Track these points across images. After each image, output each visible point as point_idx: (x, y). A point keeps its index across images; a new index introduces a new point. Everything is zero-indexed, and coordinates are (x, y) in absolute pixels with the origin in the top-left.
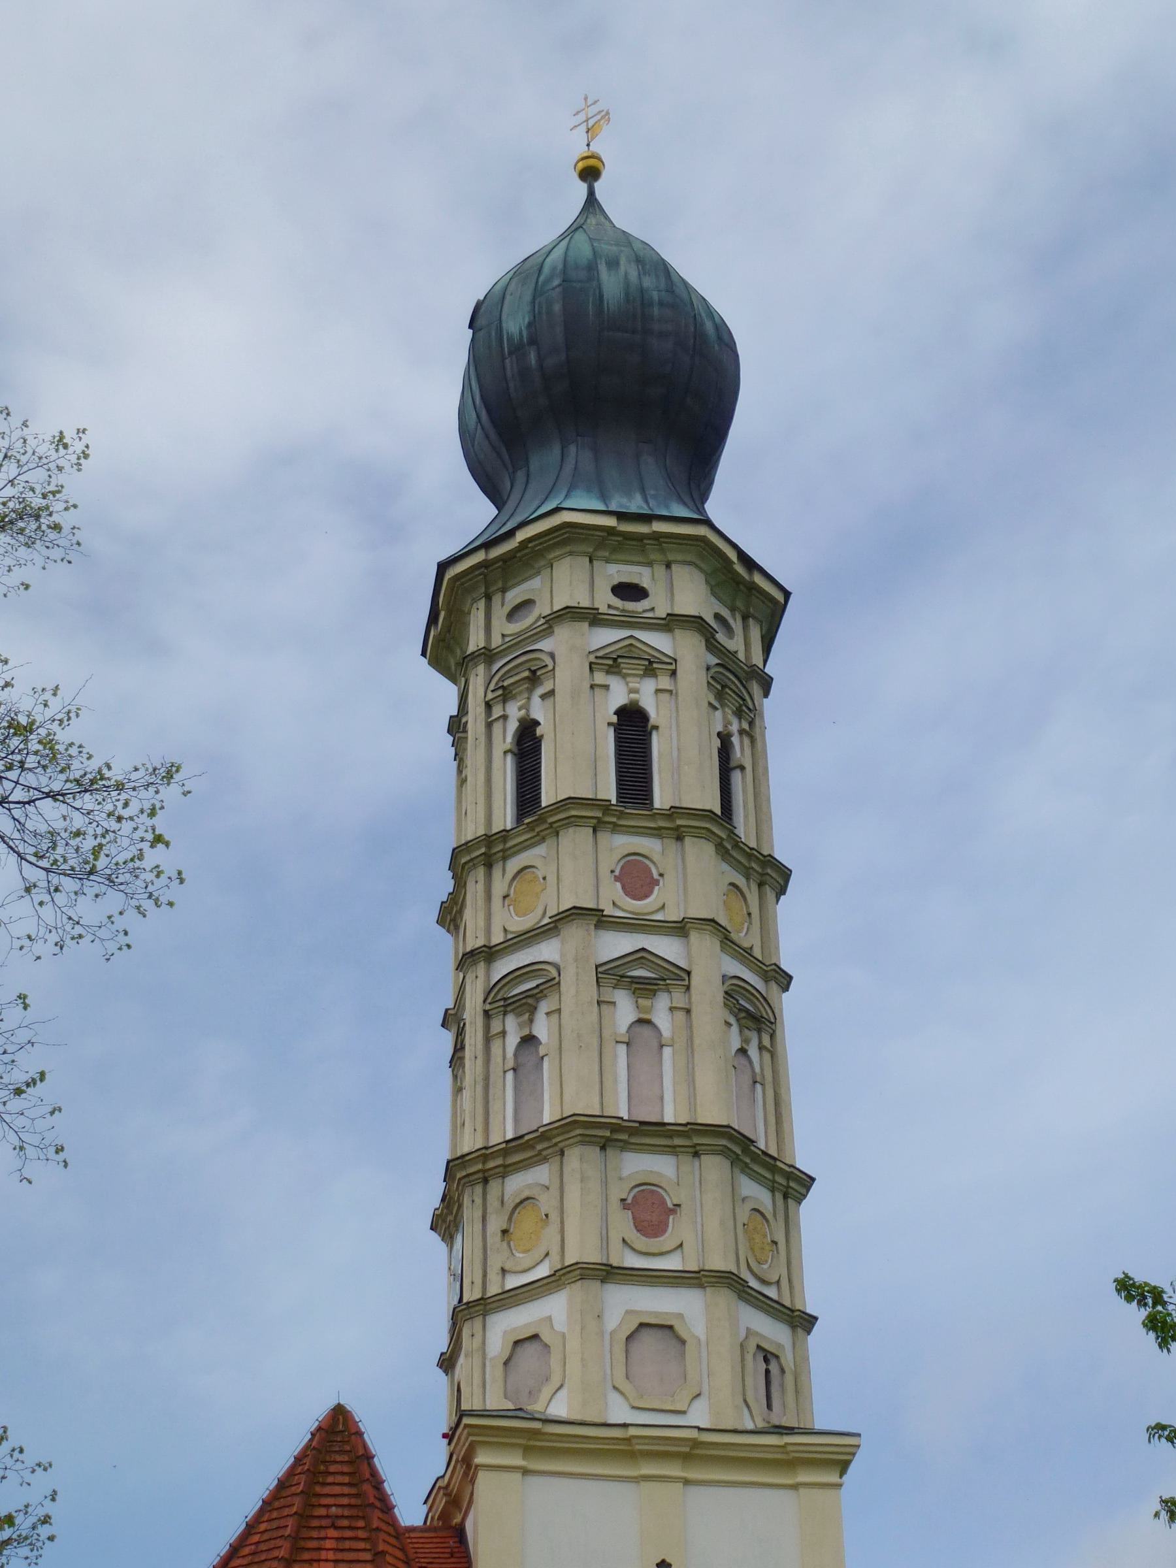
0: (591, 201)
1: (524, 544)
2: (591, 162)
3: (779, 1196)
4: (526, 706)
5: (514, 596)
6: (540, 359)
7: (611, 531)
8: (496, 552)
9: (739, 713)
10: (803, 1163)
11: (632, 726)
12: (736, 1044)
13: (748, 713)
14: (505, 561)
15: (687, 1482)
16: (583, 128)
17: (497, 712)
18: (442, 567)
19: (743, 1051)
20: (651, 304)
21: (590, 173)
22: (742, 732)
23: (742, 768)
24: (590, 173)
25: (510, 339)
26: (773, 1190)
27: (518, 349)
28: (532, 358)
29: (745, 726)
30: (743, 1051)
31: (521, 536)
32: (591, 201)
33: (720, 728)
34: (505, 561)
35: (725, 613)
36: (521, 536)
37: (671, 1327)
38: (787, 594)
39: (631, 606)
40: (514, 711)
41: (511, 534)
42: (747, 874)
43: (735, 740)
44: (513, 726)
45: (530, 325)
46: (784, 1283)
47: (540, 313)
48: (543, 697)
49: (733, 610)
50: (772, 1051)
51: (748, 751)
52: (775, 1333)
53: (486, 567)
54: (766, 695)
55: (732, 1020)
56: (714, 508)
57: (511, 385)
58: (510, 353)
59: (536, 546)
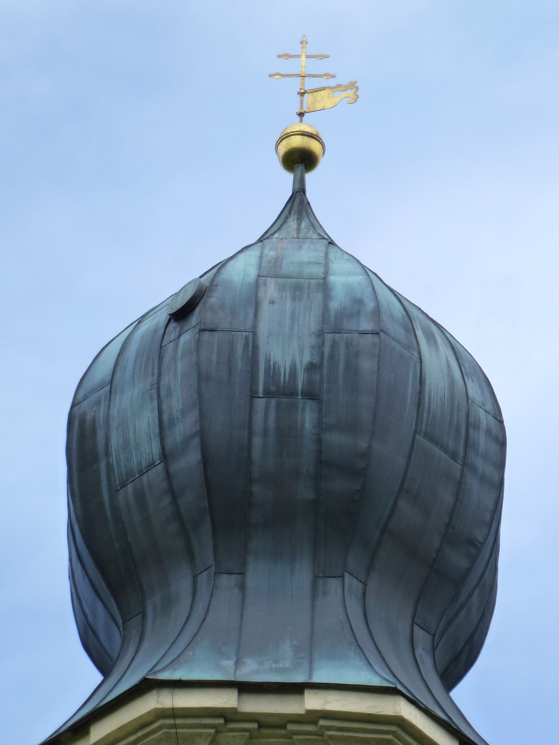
0: (298, 204)
2: (315, 146)
6: (321, 426)
7: (227, 716)
14: (261, 726)
16: (295, 84)
20: (477, 427)
21: (300, 160)
24: (300, 160)
27: (283, 392)
28: (307, 417)
31: (313, 702)
32: (298, 204)
34: (261, 726)
36: (313, 702)
41: (297, 689)
45: (311, 368)
47: (332, 356)
53: (227, 720)
57: (257, 441)
58: (268, 394)
59: (329, 728)
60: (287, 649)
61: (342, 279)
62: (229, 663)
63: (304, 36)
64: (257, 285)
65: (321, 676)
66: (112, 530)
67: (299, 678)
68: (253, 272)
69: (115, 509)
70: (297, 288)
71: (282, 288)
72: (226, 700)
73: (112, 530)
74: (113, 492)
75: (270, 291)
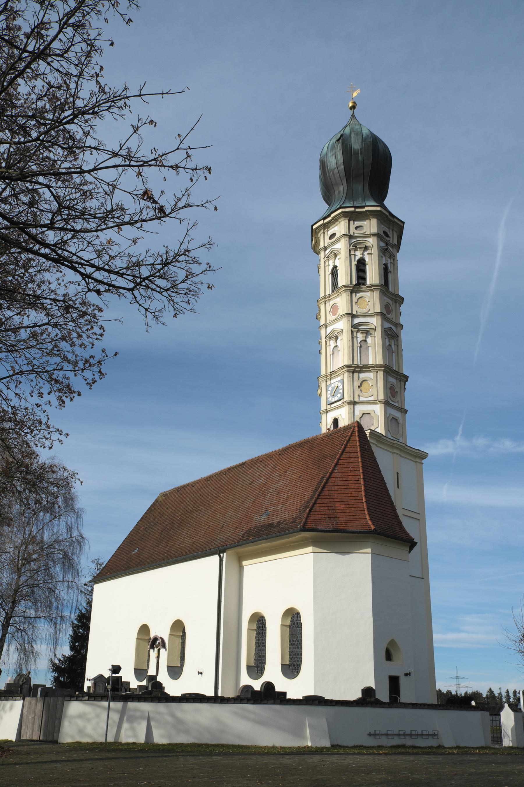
0: (353, 116)
1: (367, 211)
3: (398, 381)
4: (334, 262)
5: (331, 232)
8: (357, 210)
9: (390, 258)
10: (405, 373)
11: (361, 265)
12: (388, 344)
13: (393, 257)
15: (401, 456)
17: (327, 264)
18: (312, 226)
19: (390, 345)
22: (391, 263)
23: (391, 272)
25: (354, 150)
26: (397, 379)
29: (392, 261)
30: (390, 345)
31: (366, 209)
32: (353, 116)
33: (384, 262)
35: (387, 230)
36: (366, 209)
37: (363, 414)
38: (404, 223)
39: (336, 237)
40: (331, 264)
41: (363, 207)
42: (392, 299)
43: (389, 265)
44: (331, 267)
46: (400, 402)
48: (339, 259)
49: (389, 228)
50: (398, 345)
51: (392, 269)
52: (397, 414)
54: (398, 252)
55: (386, 337)
56: (387, 202)
60: (360, 199)
61: (365, 132)
62: (352, 203)
63: (42, 397)
64: (350, 134)
65: (367, 204)
66: (461, 426)
67: (364, 205)
68: (349, 131)
69: (329, 176)
70: (357, 134)
71: (355, 134)
72: (353, 209)
73: (461, 426)
74: (329, 173)
75: (353, 135)
